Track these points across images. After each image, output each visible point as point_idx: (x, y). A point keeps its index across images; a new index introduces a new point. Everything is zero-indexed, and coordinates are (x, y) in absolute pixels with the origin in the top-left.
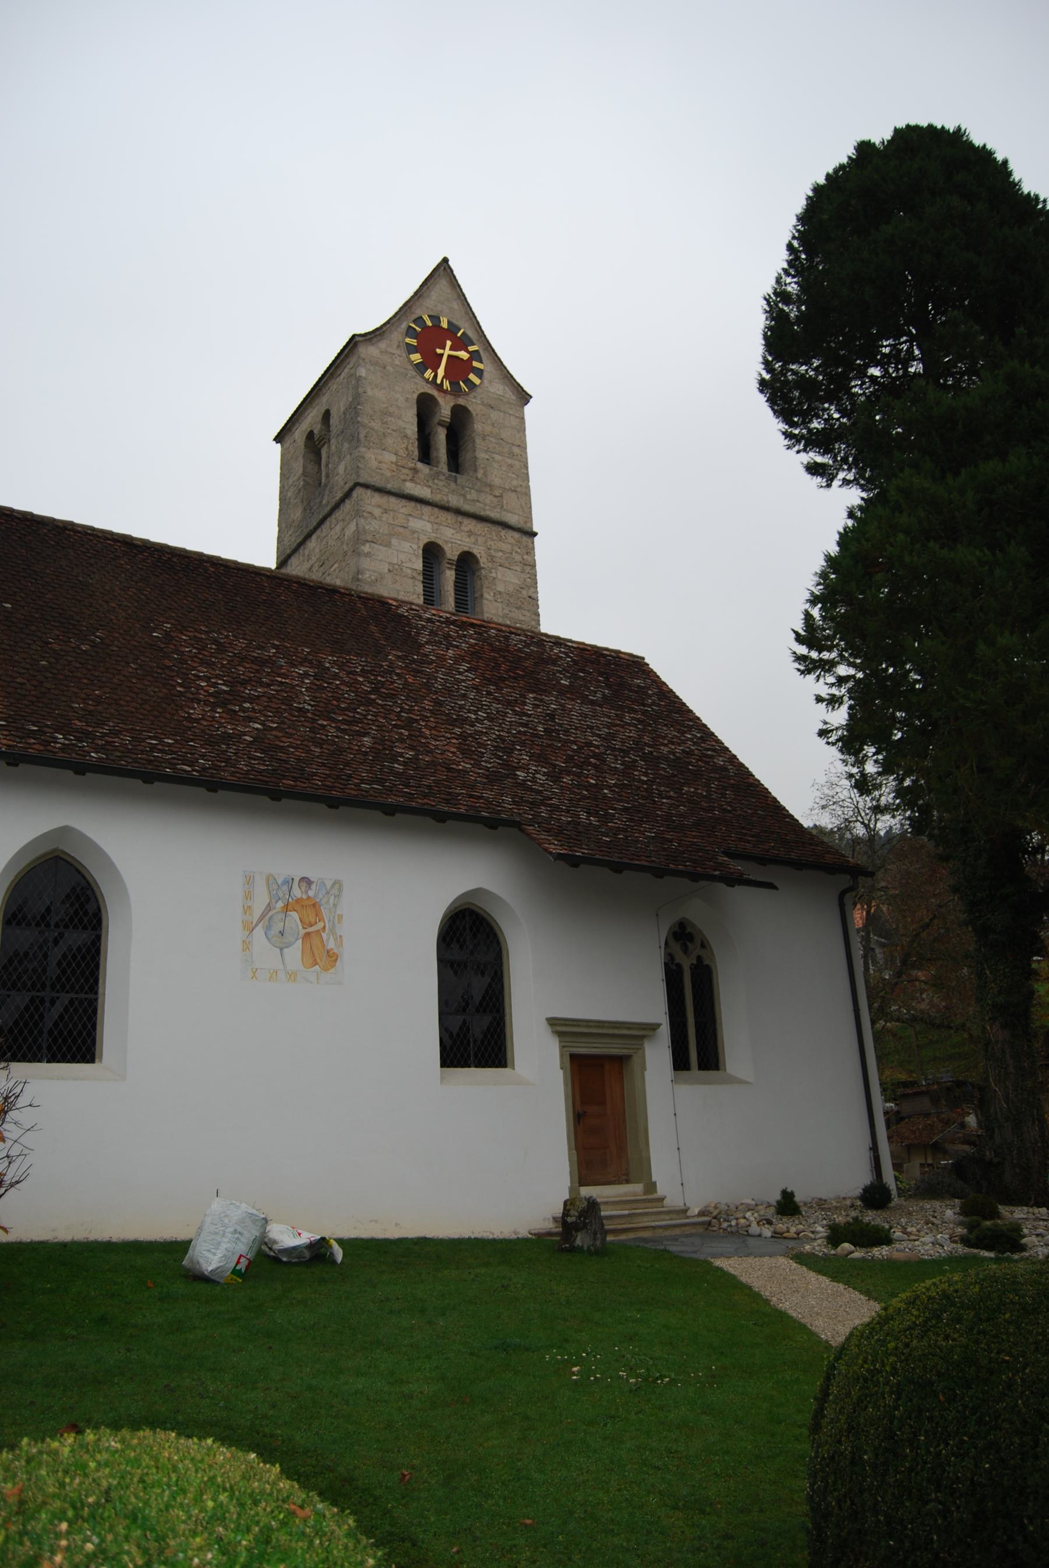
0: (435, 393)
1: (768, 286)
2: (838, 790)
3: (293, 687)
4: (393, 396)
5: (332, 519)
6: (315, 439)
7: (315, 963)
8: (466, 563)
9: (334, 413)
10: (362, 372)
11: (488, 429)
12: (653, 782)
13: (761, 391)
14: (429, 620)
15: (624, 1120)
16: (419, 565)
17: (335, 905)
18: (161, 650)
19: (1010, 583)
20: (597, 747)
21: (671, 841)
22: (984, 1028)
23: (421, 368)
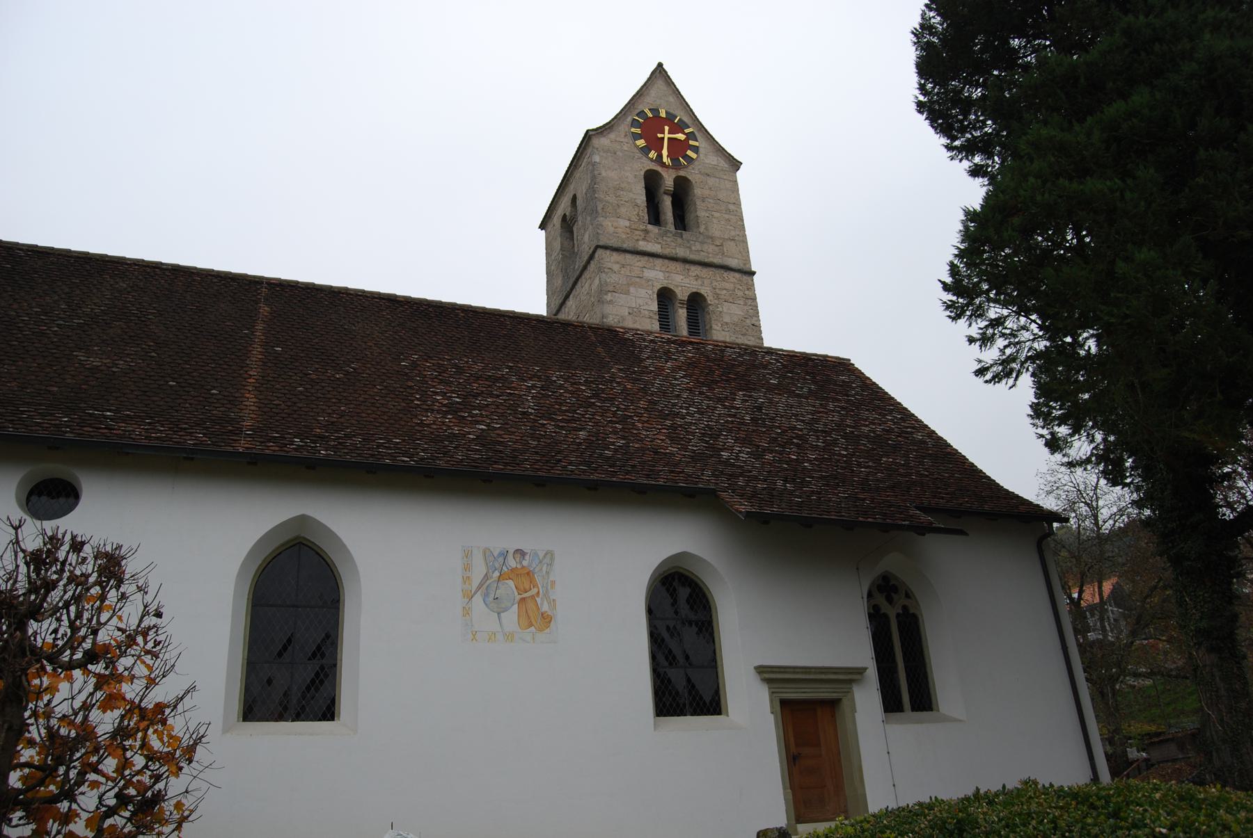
0: (659, 169)
1: (916, 22)
2: (1060, 476)
3: (520, 396)
4: (625, 177)
5: (583, 279)
6: (566, 220)
7: (531, 625)
8: (696, 303)
9: (578, 196)
10: (597, 158)
11: (707, 192)
12: (853, 455)
13: (919, 112)
14: (652, 341)
15: (839, 761)
16: (654, 307)
17: (548, 573)
18: (406, 374)
19: (1143, 203)
20: (801, 430)
21: (864, 500)
22: (1191, 653)
23: (645, 151)
